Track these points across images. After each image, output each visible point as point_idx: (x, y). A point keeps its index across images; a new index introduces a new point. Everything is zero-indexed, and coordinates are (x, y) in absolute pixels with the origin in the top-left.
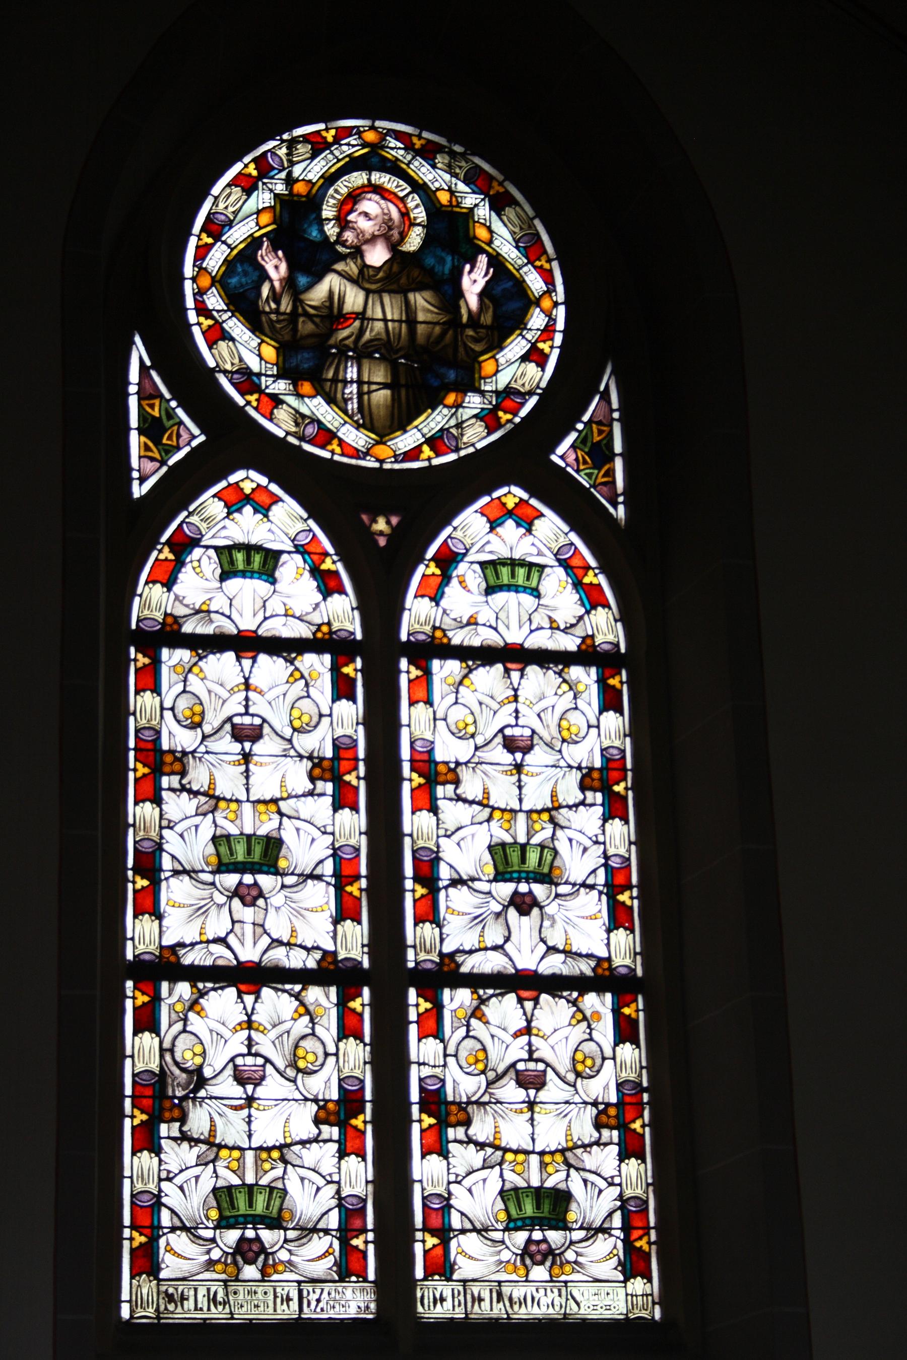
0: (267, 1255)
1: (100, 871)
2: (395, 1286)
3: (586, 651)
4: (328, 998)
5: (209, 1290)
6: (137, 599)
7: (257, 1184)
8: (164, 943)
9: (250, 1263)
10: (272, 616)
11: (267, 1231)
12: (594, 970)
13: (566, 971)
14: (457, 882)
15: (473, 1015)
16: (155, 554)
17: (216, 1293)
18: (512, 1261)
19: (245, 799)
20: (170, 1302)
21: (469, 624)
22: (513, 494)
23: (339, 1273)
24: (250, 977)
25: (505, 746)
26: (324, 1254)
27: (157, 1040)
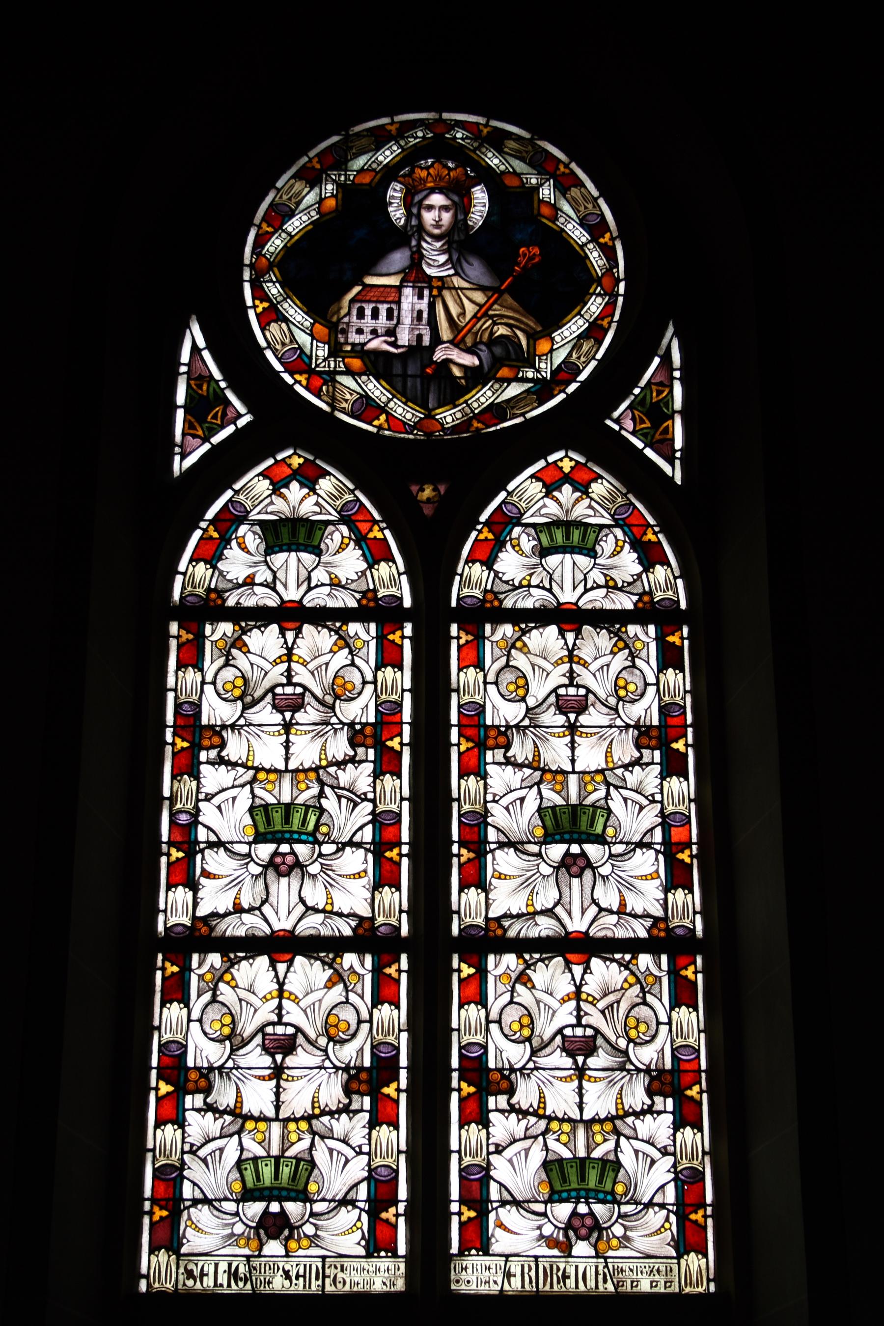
0: (292, 1228)
1: (138, 844)
2: (430, 1260)
3: (643, 609)
4: (363, 965)
5: (230, 1265)
6: (457, 578)
7: (588, 1157)
8: (491, 915)
9: (583, 1239)
10: (317, 586)
11: (600, 1205)
12: (354, 930)
13: (325, 932)
14: (217, 844)
15: (518, 979)
16: (474, 534)
17: (237, 1268)
18: (246, 1234)
19: (570, 769)
20: (188, 1279)
21: (245, 584)
22: (565, 460)
23: (366, 1248)
24: (577, 948)
25: (274, 706)
26: (656, 1231)
27: (483, 1012)
